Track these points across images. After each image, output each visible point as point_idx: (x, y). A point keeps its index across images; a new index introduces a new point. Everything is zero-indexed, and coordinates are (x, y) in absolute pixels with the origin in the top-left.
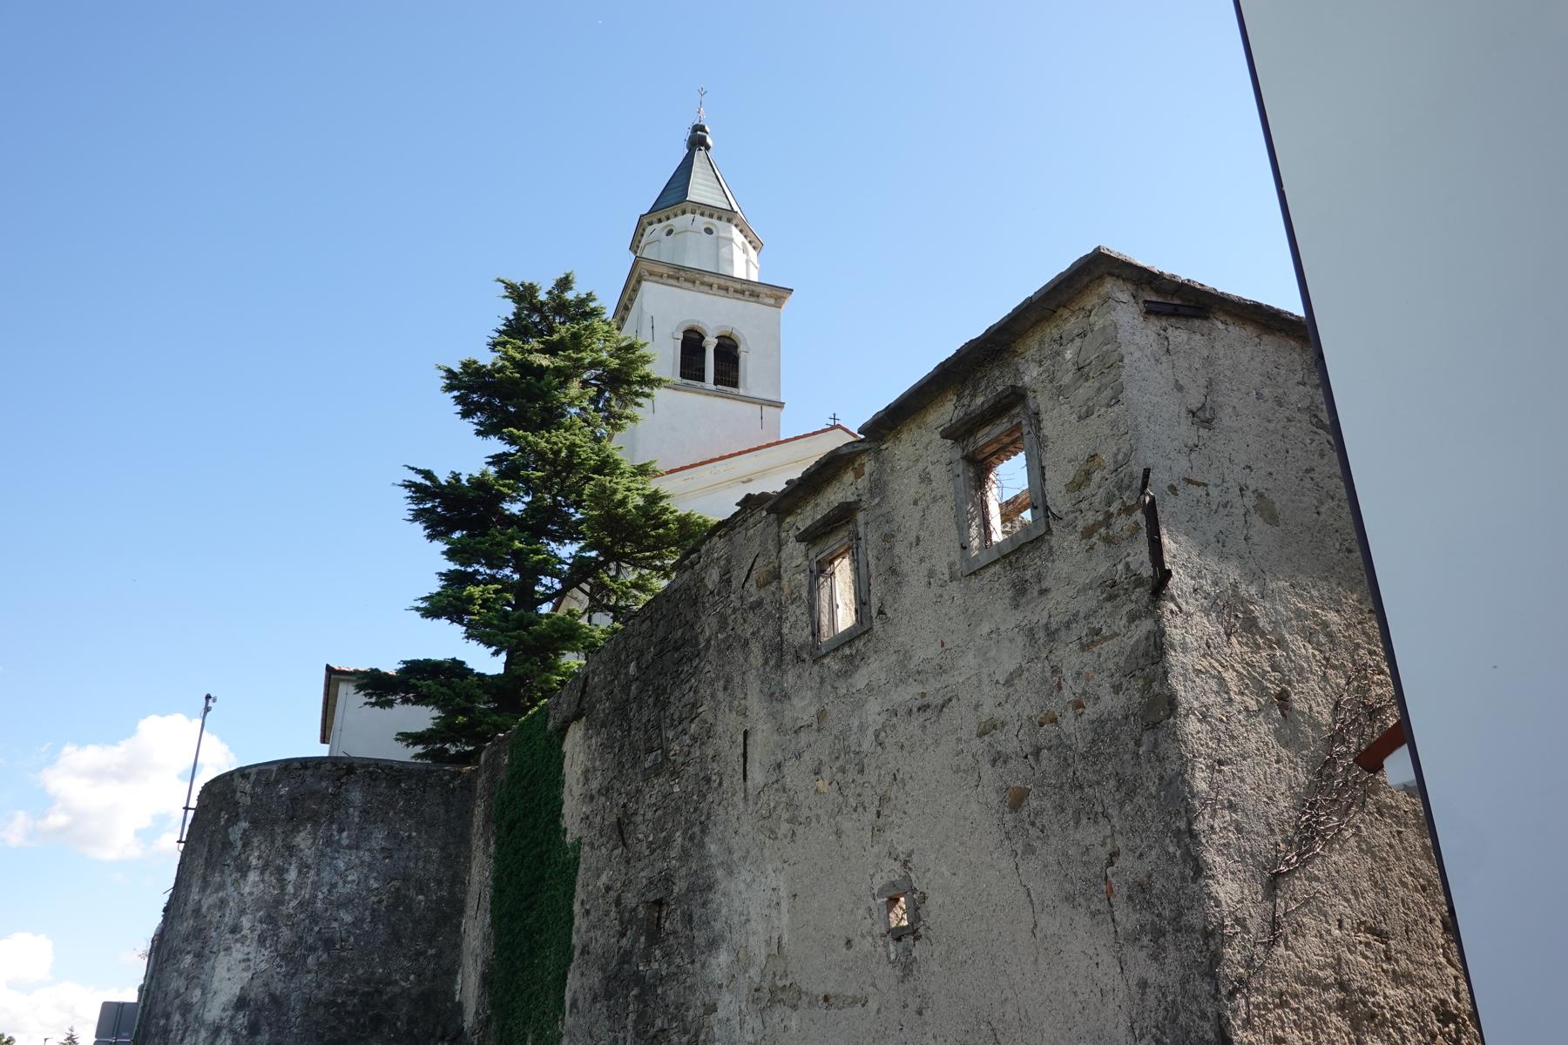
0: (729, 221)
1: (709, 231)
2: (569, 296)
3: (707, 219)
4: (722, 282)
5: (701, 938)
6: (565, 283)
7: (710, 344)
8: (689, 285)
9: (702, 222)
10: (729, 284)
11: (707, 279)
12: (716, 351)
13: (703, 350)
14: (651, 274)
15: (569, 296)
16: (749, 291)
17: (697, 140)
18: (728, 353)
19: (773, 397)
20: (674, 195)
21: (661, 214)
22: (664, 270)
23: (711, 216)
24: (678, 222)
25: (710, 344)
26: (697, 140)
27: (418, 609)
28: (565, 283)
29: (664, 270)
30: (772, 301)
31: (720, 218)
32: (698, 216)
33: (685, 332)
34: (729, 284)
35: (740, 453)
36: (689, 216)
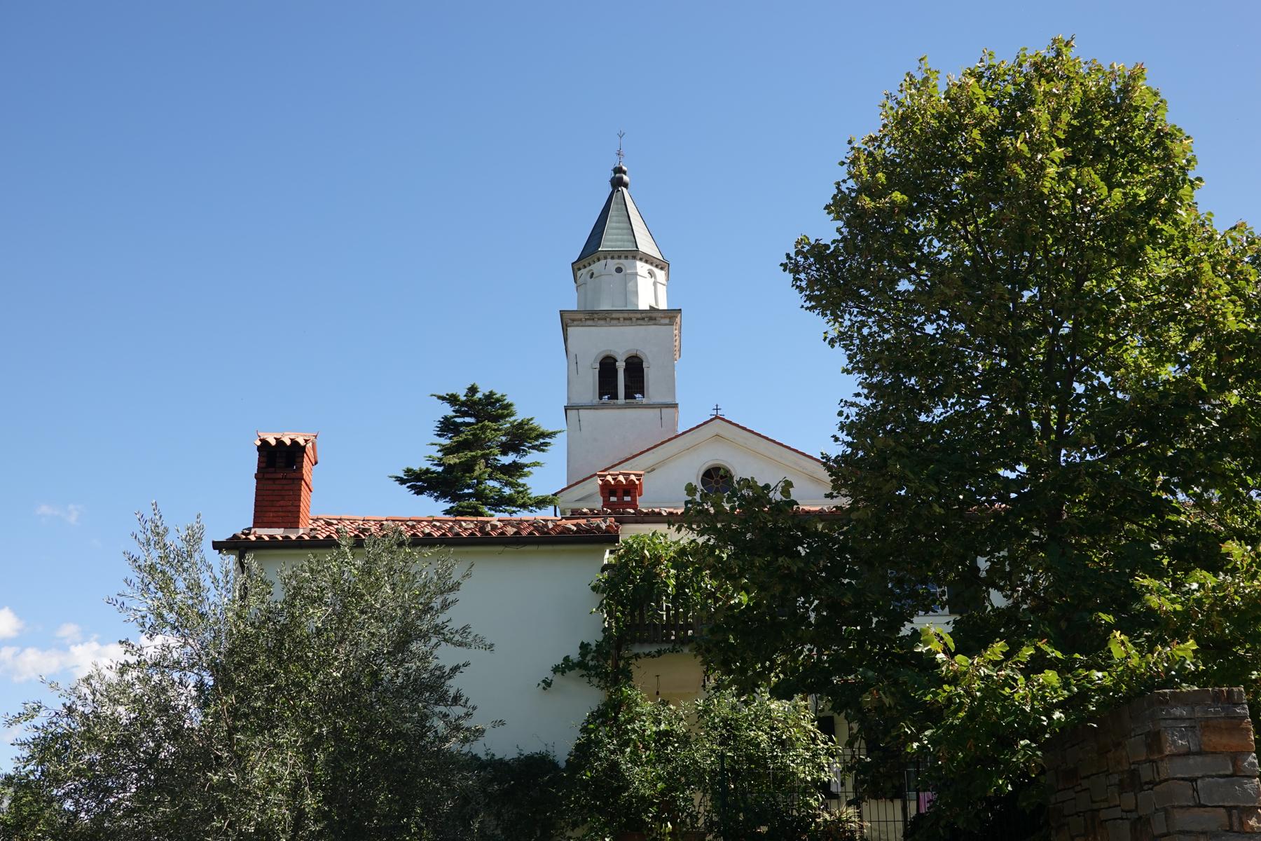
0: (634, 258)
1: (619, 270)
2: (479, 395)
3: (616, 261)
4: (626, 315)
5: (777, 496)
6: (473, 390)
7: (621, 366)
8: (602, 322)
9: (612, 264)
10: (631, 315)
11: (614, 316)
12: (625, 370)
13: (616, 371)
14: (573, 320)
15: (479, 395)
16: (652, 316)
17: (617, 183)
18: (635, 367)
19: (669, 400)
20: (592, 250)
21: (585, 262)
22: (581, 316)
23: (619, 257)
24: (597, 267)
25: (621, 366)
26: (617, 183)
27: (543, 435)
28: (473, 390)
29: (581, 316)
30: (667, 321)
31: (626, 257)
32: (609, 261)
33: (601, 364)
34: (631, 315)
35: (642, 453)
36: (603, 262)
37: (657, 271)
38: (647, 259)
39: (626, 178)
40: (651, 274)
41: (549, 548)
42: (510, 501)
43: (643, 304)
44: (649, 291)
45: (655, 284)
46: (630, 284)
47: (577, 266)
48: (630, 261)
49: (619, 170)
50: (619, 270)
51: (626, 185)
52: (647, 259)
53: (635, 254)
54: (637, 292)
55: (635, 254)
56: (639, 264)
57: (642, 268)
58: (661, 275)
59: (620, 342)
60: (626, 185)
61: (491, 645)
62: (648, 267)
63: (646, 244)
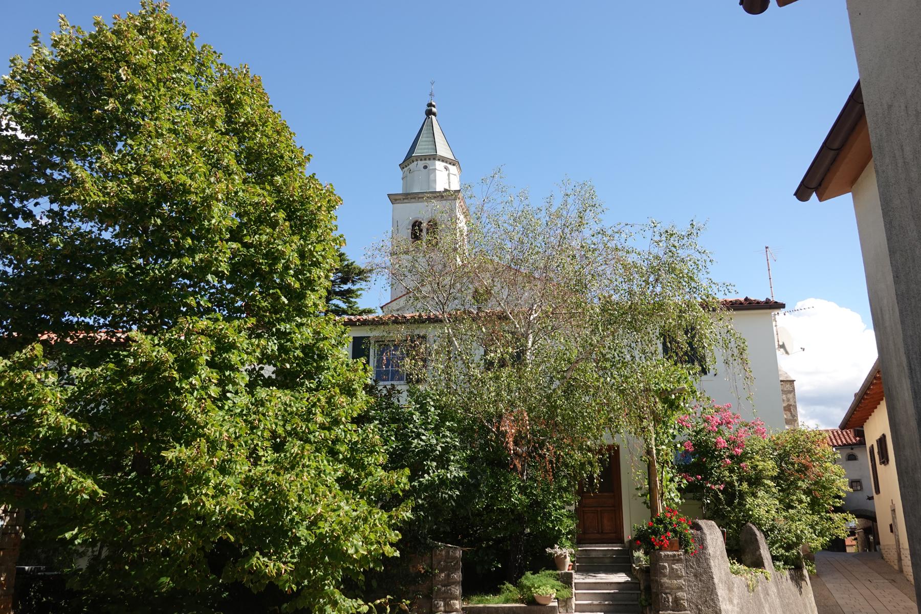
0: (434, 159)
1: (425, 167)
3: (423, 162)
7: (424, 225)
9: (421, 164)
18: (433, 225)
20: (409, 158)
21: (408, 162)
22: (401, 197)
24: (412, 166)
26: (429, 113)
29: (401, 197)
32: (419, 162)
36: (415, 163)
37: (450, 166)
38: (443, 159)
39: (434, 109)
40: (446, 168)
41: (860, 179)
42: (345, 312)
43: (440, 187)
44: (445, 178)
45: (449, 175)
46: (432, 176)
47: (403, 166)
48: (432, 161)
49: (430, 105)
50: (425, 167)
51: (434, 114)
52: (443, 159)
53: (434, 157)
54: (435, 181)
55: (434, 157)
56: (437, 163)
57: (439, 165)
58: (453, 169)
59: (422, 211)
60: (434, 114)
61: (12, 61)
62: (445, 164)
63: (443, 149)
